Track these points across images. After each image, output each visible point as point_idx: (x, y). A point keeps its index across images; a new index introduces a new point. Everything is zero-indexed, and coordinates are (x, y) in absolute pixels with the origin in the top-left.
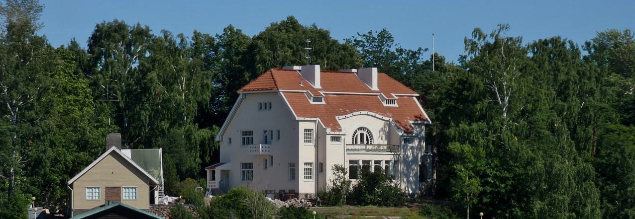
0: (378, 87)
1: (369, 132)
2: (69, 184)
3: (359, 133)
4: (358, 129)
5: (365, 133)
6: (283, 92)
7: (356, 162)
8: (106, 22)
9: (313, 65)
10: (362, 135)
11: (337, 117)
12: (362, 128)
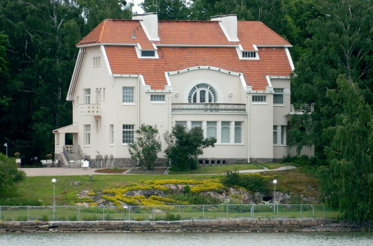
1: (211, 89)
3: (198, 91)
10: (203, 93)
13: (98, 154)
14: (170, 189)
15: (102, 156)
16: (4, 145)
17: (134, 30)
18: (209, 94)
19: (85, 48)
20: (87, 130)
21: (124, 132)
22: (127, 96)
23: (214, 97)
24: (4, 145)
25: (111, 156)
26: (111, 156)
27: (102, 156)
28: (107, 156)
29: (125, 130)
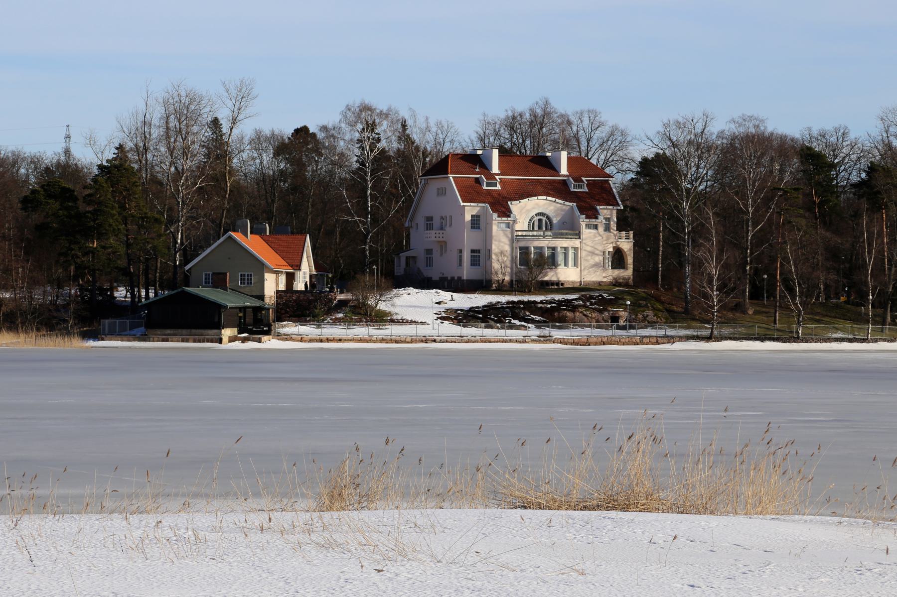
0: (499, 168)
1: (548, 217)
2: (187, 269)
3: (536, 219)
4: (536, 215)
5: (544, 219)
6: (453, 177)
7: (541, 248)
8: (671, 120)
9: (559, 152)
10: (540, 220)
11: (509, 203)
12: (540, 213)
13: (441, 276)
14: (547, 276)
15: (447, 278)
16: (373, 267)
17: (778, 425)
18: (546, 221)
19: (428, 179)
20: (427, 254)
21: (471, 256)
22: (477, 224)
23: (550, 227)
24: (373, 267)
25: (458, 277)
26: (458, 277)
27: (447, 278)
28: (454, 277)
29: (478, 254)
